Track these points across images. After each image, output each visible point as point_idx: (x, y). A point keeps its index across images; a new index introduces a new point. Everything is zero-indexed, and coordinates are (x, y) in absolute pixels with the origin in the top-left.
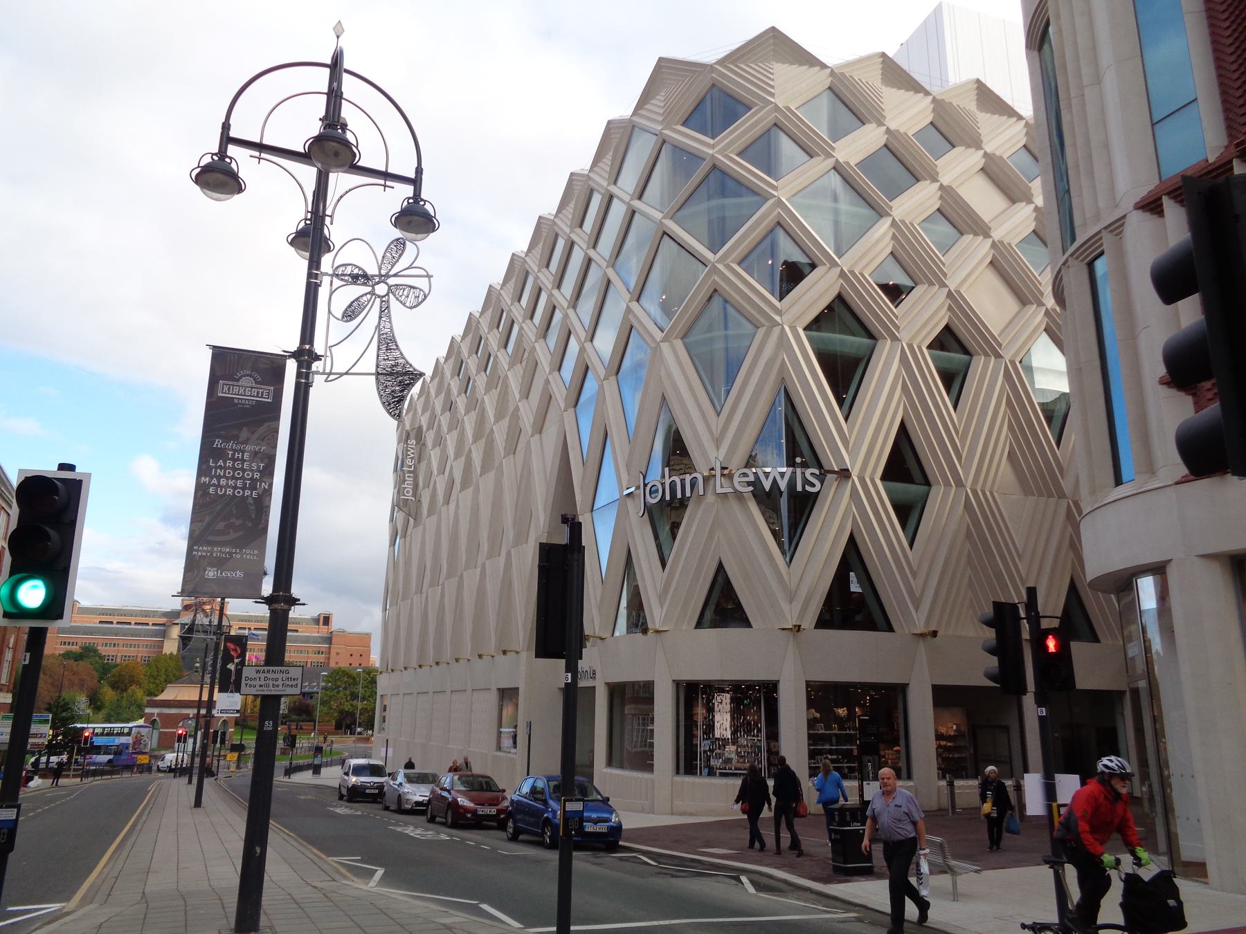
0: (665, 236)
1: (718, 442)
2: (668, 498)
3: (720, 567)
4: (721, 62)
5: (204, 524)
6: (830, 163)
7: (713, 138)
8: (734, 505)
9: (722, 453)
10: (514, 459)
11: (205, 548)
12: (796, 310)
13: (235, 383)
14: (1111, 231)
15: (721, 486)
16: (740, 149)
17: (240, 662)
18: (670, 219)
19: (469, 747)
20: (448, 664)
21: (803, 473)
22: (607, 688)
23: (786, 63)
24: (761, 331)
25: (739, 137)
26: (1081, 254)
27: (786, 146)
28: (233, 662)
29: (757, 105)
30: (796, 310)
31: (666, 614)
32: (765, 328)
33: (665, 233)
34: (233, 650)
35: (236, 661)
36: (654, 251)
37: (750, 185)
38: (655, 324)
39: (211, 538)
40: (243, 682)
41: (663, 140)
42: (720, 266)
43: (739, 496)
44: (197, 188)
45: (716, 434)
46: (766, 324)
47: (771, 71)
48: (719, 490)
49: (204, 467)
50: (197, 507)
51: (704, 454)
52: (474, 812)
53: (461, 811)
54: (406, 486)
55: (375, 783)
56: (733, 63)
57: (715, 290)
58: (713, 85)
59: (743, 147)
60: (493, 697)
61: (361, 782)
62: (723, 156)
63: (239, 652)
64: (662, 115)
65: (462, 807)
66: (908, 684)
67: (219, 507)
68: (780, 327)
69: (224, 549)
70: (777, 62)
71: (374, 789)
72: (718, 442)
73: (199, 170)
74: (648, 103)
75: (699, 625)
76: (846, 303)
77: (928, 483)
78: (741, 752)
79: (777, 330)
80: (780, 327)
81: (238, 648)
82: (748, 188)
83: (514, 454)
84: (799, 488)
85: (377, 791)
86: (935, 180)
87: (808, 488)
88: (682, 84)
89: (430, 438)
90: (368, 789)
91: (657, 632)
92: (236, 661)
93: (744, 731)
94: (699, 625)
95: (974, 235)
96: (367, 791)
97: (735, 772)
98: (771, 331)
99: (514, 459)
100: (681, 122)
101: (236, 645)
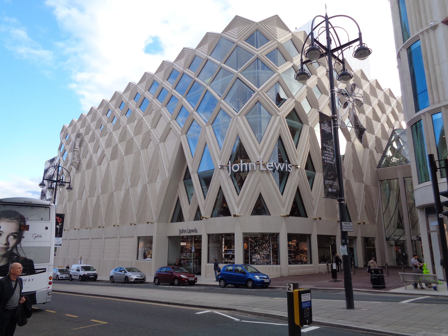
0: (238, 79)
1: (260, 153)
2: (242, 170)
3: (260, 194)
4: (260, 22)
5: (326, 172)
6: (292, 64)
7: (257, 48)
8: (266, 174)
9: (262, 156)
10: (147, 151)
11: (327, 181)
12: (283, 111)
13: (324, 125)
14: (444, 107)
15: (262, 168)
16: (266, 54)
17: (61, 225)
18: (240, 73)
19: (119, 259)
20: (103, 227)
21: (288, 166)
22: (138, 238)
23: (282, 29)
24: (273, 117)
25: (266, 50)
26: (430, 112)
27: (280, 57)
28: (59, 225)
29: (272, 40)
30: (283, 111)
31: (240, 211)
32: (275, 116)
33: (238, 78)
34: (59, 220)
35: (60, 224)
36: (233, 83)
37: (268, 66)
38: (233, 109)
39: (328, 178)
40: (343, 227)
41: (237, 45)
42: (260, 93)
43: (267, 171)
44: (356, 59)
45: (260, 150)
46: (275, 115)
47: (276, 29)
48: (261, 169)
49: (323, 153)
50: (323, 167)
51: (255, 156)
52: (188, 279)
53: (183, 279)
54: (75, 156)
55: (93, 273)
56: (264, 24)
57: (258, 101)
58: (257, 30)
59: (267, 53)
60: (136, 239)
61: (87, 273)
62: (261, 55)
63: (61, 221)
64: (237, 36)
65: (183, 278)
66: (311, 234)
67: (328, 167)
68: (280, 116)
69: (330, 181)
70: (278, 27)
71: (93, 276)
72: (260, 153)
73: (355, 53)
74: (229, 30)
75: (251, 215)
76: (296, 112)
77: (314, 171)
78: (264, 257)
79: (278, 117)
80: (280, 116)
81: (61, 219)
82: (267, 67)
83: (146, 148)
84: (287, 170)
85: (94, 277)
86: (316, 75)
87: (289, 170)
88: (244, 27)
89: (87, 138)
90: (91, 276)
91: (235, 216)
92: (60, 224)
93: (265, 249)
94: (251, 215)
95: (325, 95)
96: (90, 277)
97: (262, 263)
98: (276, 117)
99: (147, 151)
100: (245, 40)
101: (60, 218)
